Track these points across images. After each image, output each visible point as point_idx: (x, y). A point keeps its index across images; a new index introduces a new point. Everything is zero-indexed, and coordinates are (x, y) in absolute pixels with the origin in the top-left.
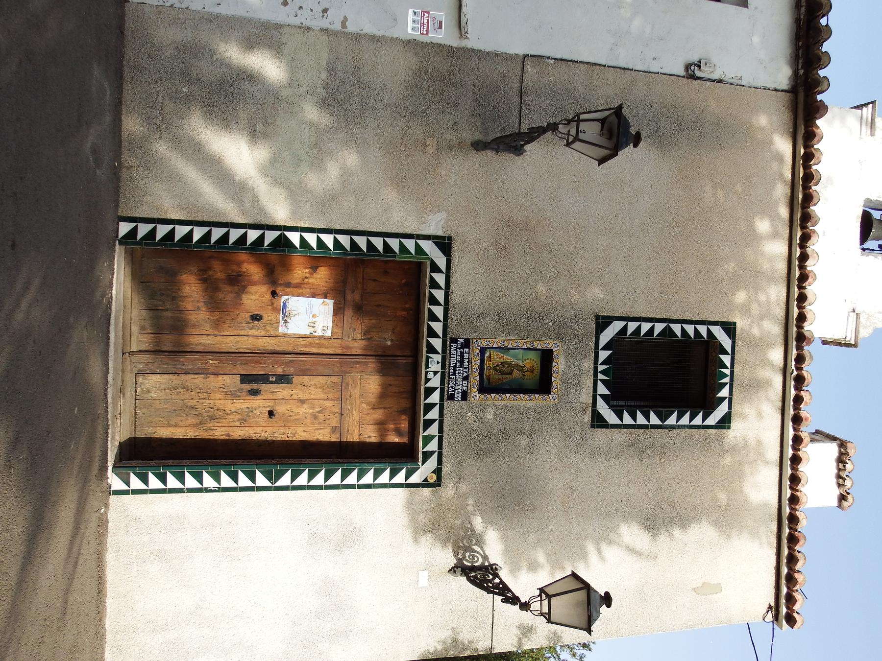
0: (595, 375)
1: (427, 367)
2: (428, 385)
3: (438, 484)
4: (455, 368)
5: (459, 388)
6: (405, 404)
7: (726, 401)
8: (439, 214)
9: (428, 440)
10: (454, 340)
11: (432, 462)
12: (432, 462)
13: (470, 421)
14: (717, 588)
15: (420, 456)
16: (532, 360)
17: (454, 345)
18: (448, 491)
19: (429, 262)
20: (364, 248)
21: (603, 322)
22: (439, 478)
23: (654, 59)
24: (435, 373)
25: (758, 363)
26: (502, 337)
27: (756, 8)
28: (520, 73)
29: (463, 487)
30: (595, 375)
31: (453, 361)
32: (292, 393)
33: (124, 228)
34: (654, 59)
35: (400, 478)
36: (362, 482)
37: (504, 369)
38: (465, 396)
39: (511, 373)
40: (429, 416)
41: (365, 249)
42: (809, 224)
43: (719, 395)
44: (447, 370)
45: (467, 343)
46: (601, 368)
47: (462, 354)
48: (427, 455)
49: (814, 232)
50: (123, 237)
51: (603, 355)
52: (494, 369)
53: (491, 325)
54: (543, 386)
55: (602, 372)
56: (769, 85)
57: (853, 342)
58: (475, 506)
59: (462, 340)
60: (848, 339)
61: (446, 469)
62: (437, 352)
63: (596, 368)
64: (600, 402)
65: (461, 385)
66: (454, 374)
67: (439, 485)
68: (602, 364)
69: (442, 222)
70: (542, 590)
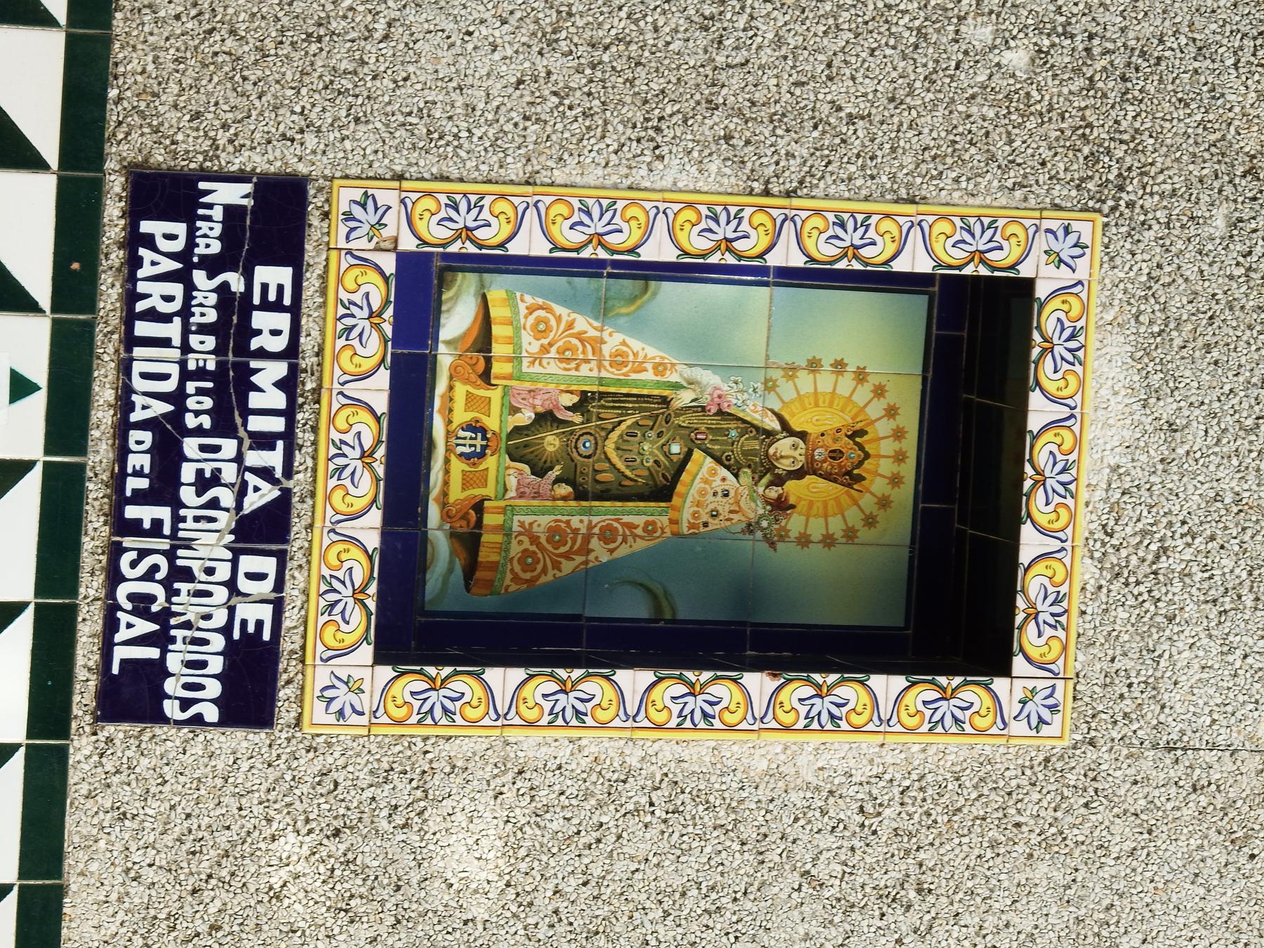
1: (115, 578)
4: (168, 437)
5: (205, 612)
10: (165, 193)
13: (296, 910)
16: (851, 376)
26: (589, 172)
37: (604, 448)
38: (251, 686)
39: (662, 489)
44: (100, 453)
45: (277, 219)
47: (234, 319)
52: (520, 446)
54: (949, 603)
65: (221, 594)
66: (164, 488)
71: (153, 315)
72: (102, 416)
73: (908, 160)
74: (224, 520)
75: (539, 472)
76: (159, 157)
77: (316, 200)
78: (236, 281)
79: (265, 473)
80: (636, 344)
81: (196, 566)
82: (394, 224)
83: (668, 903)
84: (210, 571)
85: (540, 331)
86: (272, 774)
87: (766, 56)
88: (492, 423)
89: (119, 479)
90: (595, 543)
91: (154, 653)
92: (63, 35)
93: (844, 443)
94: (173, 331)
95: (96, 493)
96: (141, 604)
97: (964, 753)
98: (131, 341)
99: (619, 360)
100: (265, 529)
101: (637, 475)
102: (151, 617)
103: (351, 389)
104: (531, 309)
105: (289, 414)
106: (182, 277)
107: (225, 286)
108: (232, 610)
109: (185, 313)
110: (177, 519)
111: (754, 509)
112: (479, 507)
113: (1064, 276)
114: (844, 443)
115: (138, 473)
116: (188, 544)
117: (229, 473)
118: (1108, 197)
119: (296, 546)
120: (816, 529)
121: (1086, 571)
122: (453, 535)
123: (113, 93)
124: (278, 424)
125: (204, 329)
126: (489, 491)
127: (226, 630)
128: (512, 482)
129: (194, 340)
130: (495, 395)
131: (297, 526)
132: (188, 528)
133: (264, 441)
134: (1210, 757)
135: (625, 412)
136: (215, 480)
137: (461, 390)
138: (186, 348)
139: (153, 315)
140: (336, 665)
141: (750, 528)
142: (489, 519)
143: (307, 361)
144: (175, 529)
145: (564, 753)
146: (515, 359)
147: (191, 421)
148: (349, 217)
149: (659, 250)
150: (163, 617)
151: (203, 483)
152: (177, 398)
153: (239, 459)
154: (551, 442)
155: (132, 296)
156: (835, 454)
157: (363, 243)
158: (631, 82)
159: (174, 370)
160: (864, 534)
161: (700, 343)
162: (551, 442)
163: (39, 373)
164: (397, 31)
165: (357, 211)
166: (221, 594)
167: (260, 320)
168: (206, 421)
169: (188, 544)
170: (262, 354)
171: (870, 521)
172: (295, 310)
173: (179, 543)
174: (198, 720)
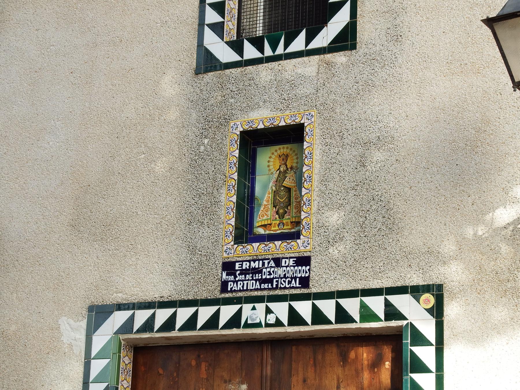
1: (285, 288)
2: (285, 321)
3: (438, 291)
6: (332, 354)
8: (62, 327)
9: (367, 314)
10: (224, 285)
11: (402, 303)
12: (402, 303)
15: (394, 323)
17: (230, 286)
18: (452, 274)
19: (122, 337)
21: (207, 63)
22: (427, 288)
24: (268, 311)
29: (449, 247)
35: (426, 354)
38: (303, 261)
39: (289, 190)
40: (331, 315)
44: (265, 293)
45: (228, 267)
46: (268, 52)
47: (244, 272)
48: (392, 313)
52: (282, 217)
53: (206, 232)
55: (274, 48)
58: (478, 221)
59: (224, 274)
61: (416, 279)
62: (239, 313)
63: (270, 59)
64: (315, 44)
65: (289, 268)
66: (270, 281)
67: (440, 287)
68: (262, 52)
69: (72, 322)
71: (243, 287)
72: (259, 293)
73: (221, 157)
74: (276, 270)
75: (286, 212)
76: (219, 288)
77: (226, 260)
78: (238, 272)
79: (269, 263)
80: (265, 198)
81: (283, 273)
82: (229, 246)
83: (342, 179)
84: (284, 271)
85: (263, 216)
86: (319, 255)
87: (205, 185)
88: (278, 222)
89: (269, 289)
90: (298, 201)
91: (298, 279)
92: (136, 311)
93: (281, 158)
94: (245, 282)
95: (272, 293)
96: (290, 282)
97: (317, 129)
98: (247, 290)
99: (268, 201)
100: (278, 262)
101: (287, 195)
102: (292, 280)
103: (255, 250)
104: (260, 218)
105: (259, 260)
107: (239, 274)
108: (291, 266)
109: (243, 281)
110: (276, 278)
112: (292, 222)
113: (239, 126)
114: (281, 158)
115: (268, 286)
116: (280, 275)
117: (268, 270)
118: (227, 121)
119: (281, 256)
120: (295, 161)
121: (288, 112)
122: (296, 226)
123: (209, 298)
124: (261, 262)
125: (245, 277)
126: (289, 221)
127: (294, 267)
128: (288, 217)
129: (247, 279)
130: (274, 222)
131: (278, 256)
132: (277, 276)
133: (263, 264)
134: (319, 83)
135: (276, 199)
136: (269, 272)
137: (273, 229)
138: (248, 280)
139: (243, 287)
140: (299, 247)
141: (295, 173)
142: (294, 221)
143: (251, 258)
144: (277, 278)
145: (316, 202)
146: (267, 220)
147: (260, 277)
148: (228, 254)
150: (292, 278)
151: (270, 274)
152: (256, 280)
153: (266, 268)
154: (281, 211)
155: (240, 291)
156: (283, 160)
157: (232, 251)
158: (209, 208)
159: (252, 281)
160: (296, 152)
161: (265, 187)
162: (281, 211)
163: (251, 305)
164: (200, 250)
165: (227, 253)
166: (289, 268)
167: (244, 268)
168: (260, 275)
169: (280, 275)
170: (250, 266)
171: (294, 151)
172: (243, 261)
173: (280, 277)
174: (309, 270)
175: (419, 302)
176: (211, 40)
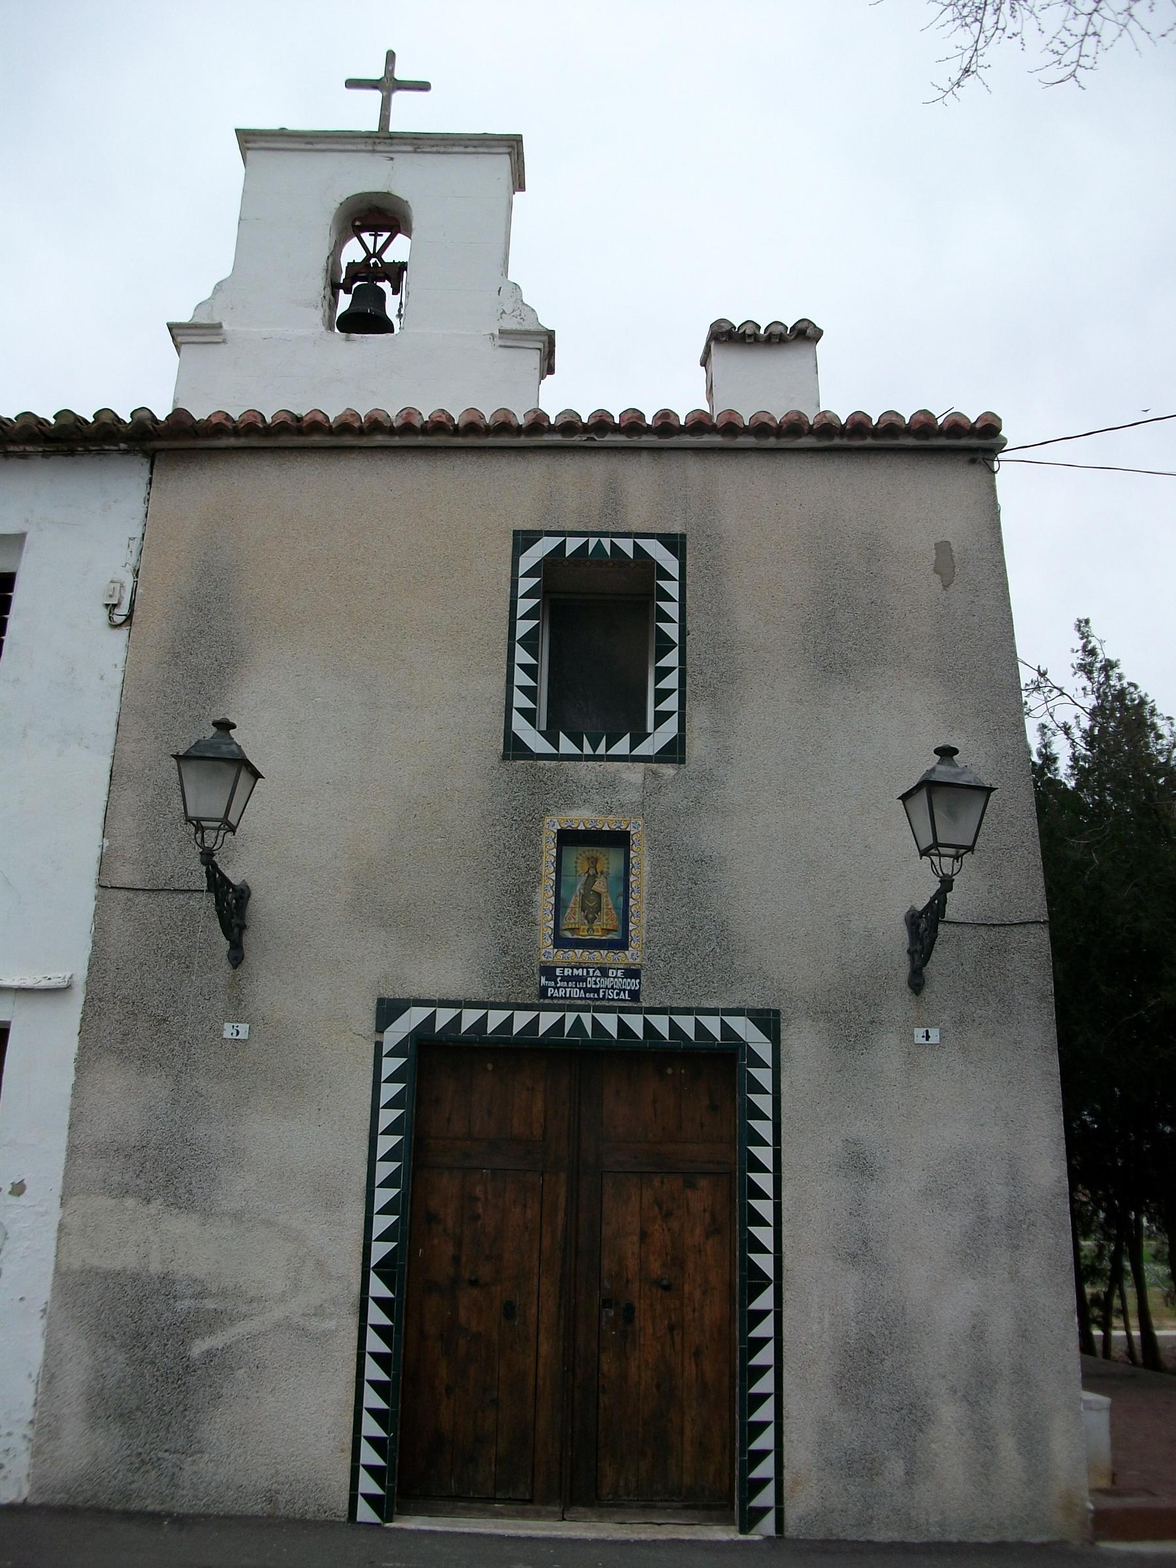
0: (600, 758)
1: (613, 999)
4: (587, 990)
5: (619, 983)
7: (641, 542)
14: (943, 548)
16: (577, 858)
20: (755, 1389)
21: (514, 748)
23: (102, 678)
25: (640, 502)
27: (27, 521)
28: (123, 891)
30: (600, 758)
31: (576, 993)
32: (630, 1254)
33: (365, 1513)
34: (102, 678)
36: (769, 1138)
38: (632, 973)
41: (754, 1390)
42: (357, 425)
43: (401, 1061)
45: (548, 971)
46: (587, 750)
49: (368, 417)
50: (380, 1514)
51: (566, 746)
56: (144, 494)
57: (546, 338)
60: (540, 346)
63: (589, 758)
66: (597, 991)
70: (924, 853)
96: (618, 994)
106: (558, 988)
111: (602, 878)
133: (588, 972)
140: (630, 956)
149: (553, 900)
154: (590, 916)
155: (562, 998)
162: (590, 916)
175: (1093, 664)
176: (520, 725)
